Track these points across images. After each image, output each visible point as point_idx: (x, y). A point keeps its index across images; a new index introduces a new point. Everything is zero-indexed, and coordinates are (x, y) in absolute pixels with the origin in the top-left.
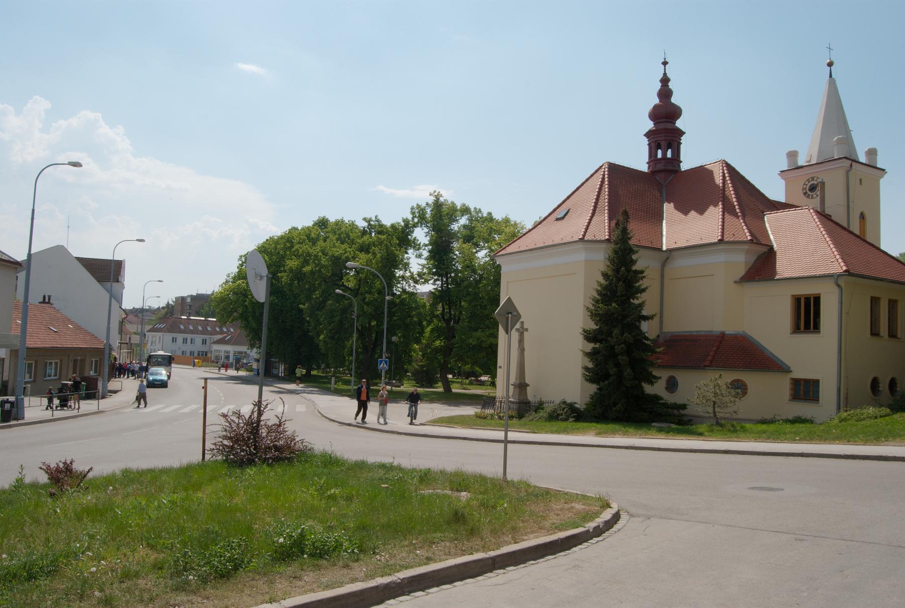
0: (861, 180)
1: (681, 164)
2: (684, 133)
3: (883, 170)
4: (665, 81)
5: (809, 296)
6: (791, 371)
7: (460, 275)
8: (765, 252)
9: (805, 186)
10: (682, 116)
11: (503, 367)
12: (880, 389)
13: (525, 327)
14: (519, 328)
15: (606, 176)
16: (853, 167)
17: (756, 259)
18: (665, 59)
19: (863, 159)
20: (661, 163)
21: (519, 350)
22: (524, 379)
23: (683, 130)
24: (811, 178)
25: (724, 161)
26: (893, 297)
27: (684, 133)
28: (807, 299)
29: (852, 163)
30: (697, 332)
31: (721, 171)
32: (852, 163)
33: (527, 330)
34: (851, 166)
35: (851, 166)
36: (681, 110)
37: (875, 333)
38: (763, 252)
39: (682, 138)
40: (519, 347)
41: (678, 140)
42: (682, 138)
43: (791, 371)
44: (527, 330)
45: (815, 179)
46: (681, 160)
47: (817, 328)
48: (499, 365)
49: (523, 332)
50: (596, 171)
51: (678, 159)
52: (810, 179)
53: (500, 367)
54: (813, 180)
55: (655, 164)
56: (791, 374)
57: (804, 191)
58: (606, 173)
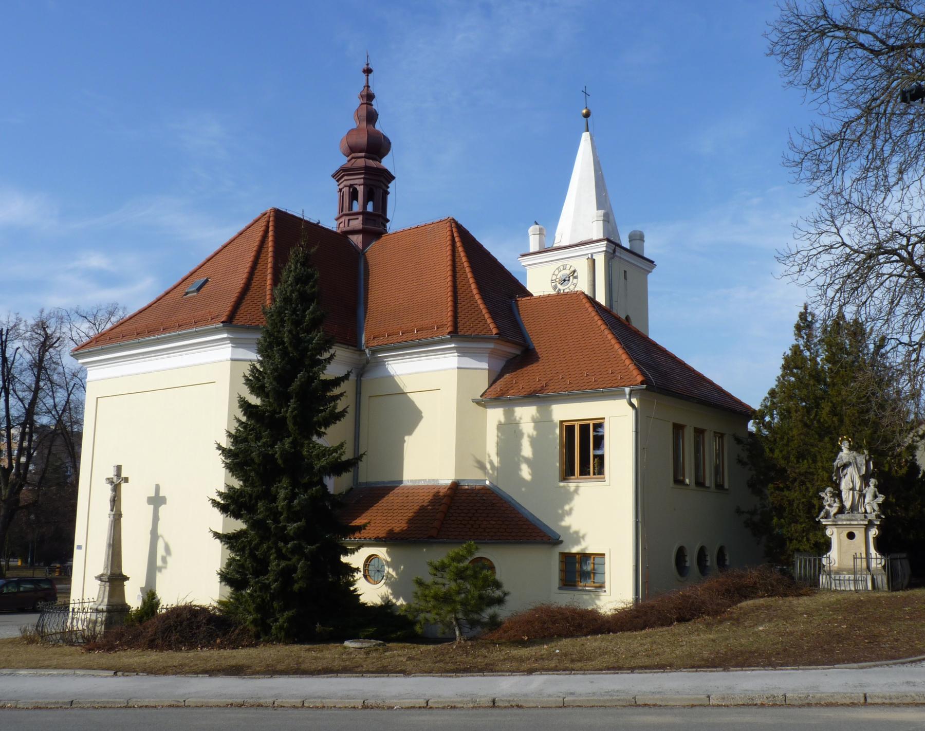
0: (625, 272)
1: (388, 225)
2: (393, 178)
3: (652, 262)
4: (369, 97)
5: (564, 428)
6: (561, 542)
7: (402, 567)
8: (518, 355)
9: (554, 277)
10: (390, 153)
11: (84, 548)
12: (688, 564)
13: (123, 475)
14: (112, 476)
15: (271, 224)
16: (617, 254)
17: (505, 366)
18: (368, 64)
19: (626, 244)
20: (358, 219)
21: (112, 517)
22: (119, 566)
23: (393, 173)
24: (563, 266)
25: (453, 219)
26: (699, 426)
27: (393, 178)
28: (584, 428)
29: (615, 248)
30: (412, 481)
31: (449, 233)
32: (615, 248)
33: (126, 480)
34: (614, 251)
35: (614, 251)
36: (390, 143)
37: (678, 481)
38: (514, 356)
39: (389, 185)
40: (112, 510)
41: (384, 187)
42: (389, 185)
43: (561, 542)
44: (126, 480)
45: (568, 267)
46: (388, 217)
47: (600, 469)
48: (76, 543)
49: (120, 484)
50: (256, 221)
51: (383, 215)
52: (562, 268)
53: (80, 547)
54: (565, 269)
55: (349, 220)
56: (561, 546)
57: (553, 284)
58: (271, 219)
